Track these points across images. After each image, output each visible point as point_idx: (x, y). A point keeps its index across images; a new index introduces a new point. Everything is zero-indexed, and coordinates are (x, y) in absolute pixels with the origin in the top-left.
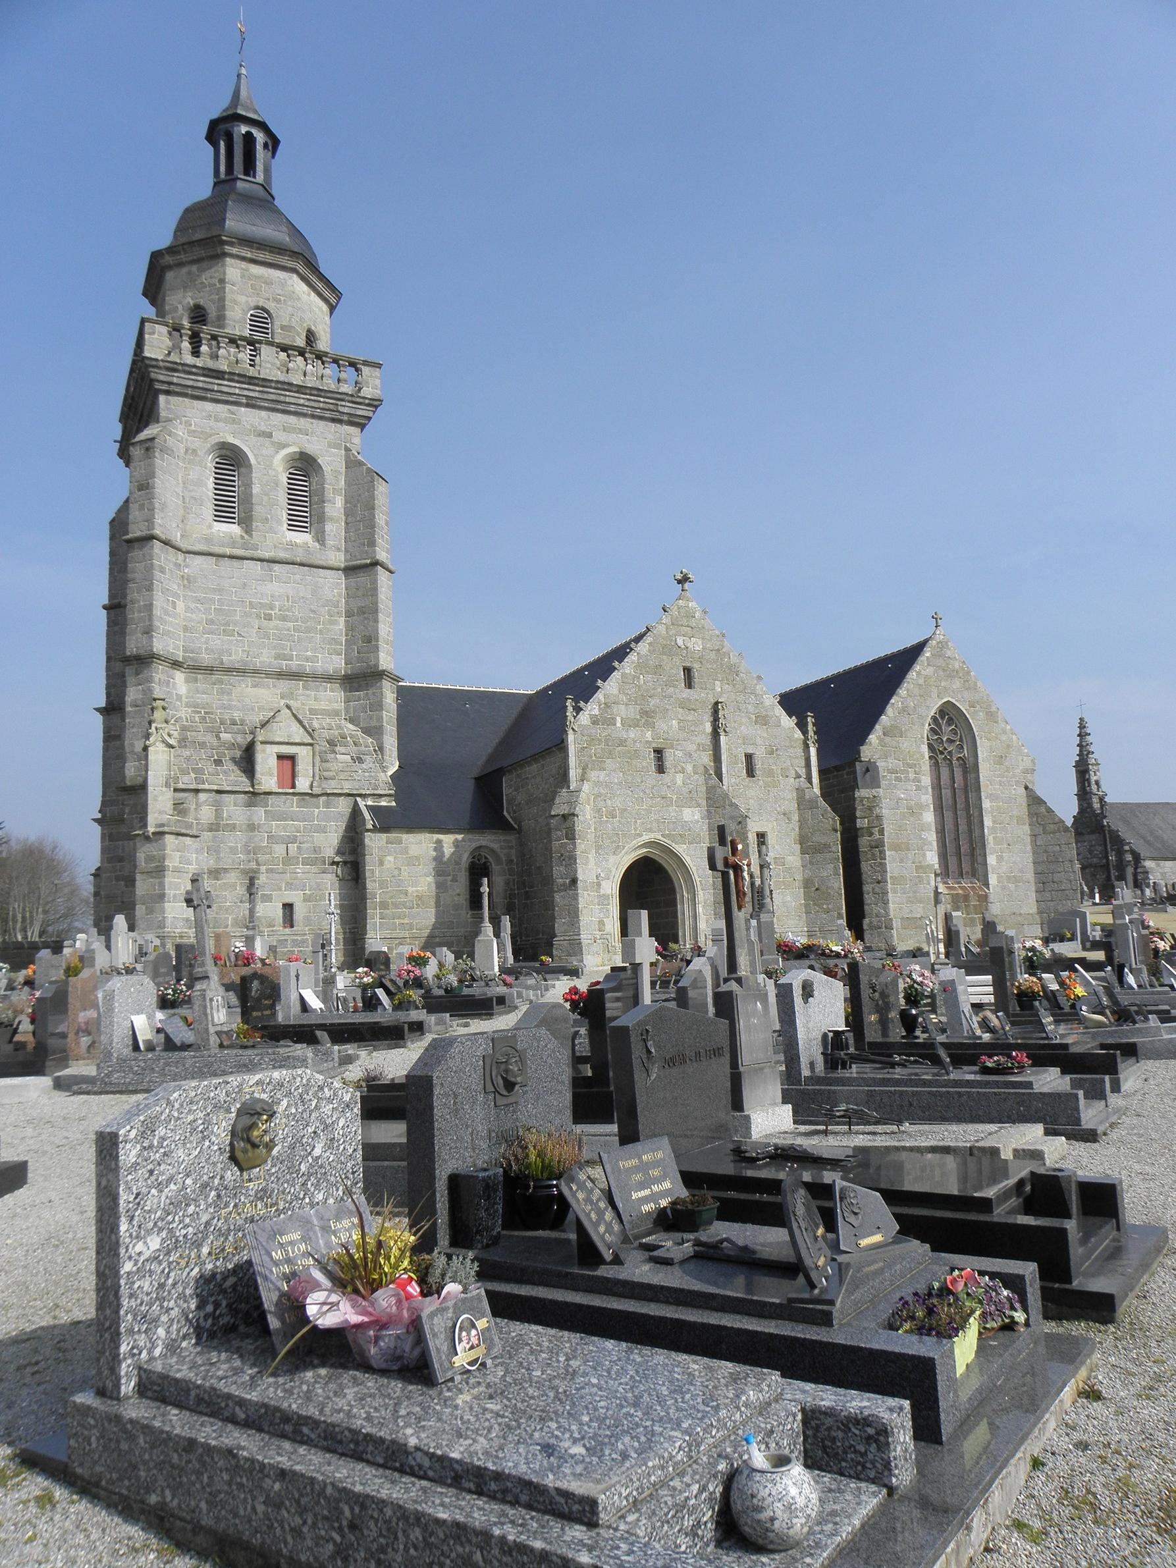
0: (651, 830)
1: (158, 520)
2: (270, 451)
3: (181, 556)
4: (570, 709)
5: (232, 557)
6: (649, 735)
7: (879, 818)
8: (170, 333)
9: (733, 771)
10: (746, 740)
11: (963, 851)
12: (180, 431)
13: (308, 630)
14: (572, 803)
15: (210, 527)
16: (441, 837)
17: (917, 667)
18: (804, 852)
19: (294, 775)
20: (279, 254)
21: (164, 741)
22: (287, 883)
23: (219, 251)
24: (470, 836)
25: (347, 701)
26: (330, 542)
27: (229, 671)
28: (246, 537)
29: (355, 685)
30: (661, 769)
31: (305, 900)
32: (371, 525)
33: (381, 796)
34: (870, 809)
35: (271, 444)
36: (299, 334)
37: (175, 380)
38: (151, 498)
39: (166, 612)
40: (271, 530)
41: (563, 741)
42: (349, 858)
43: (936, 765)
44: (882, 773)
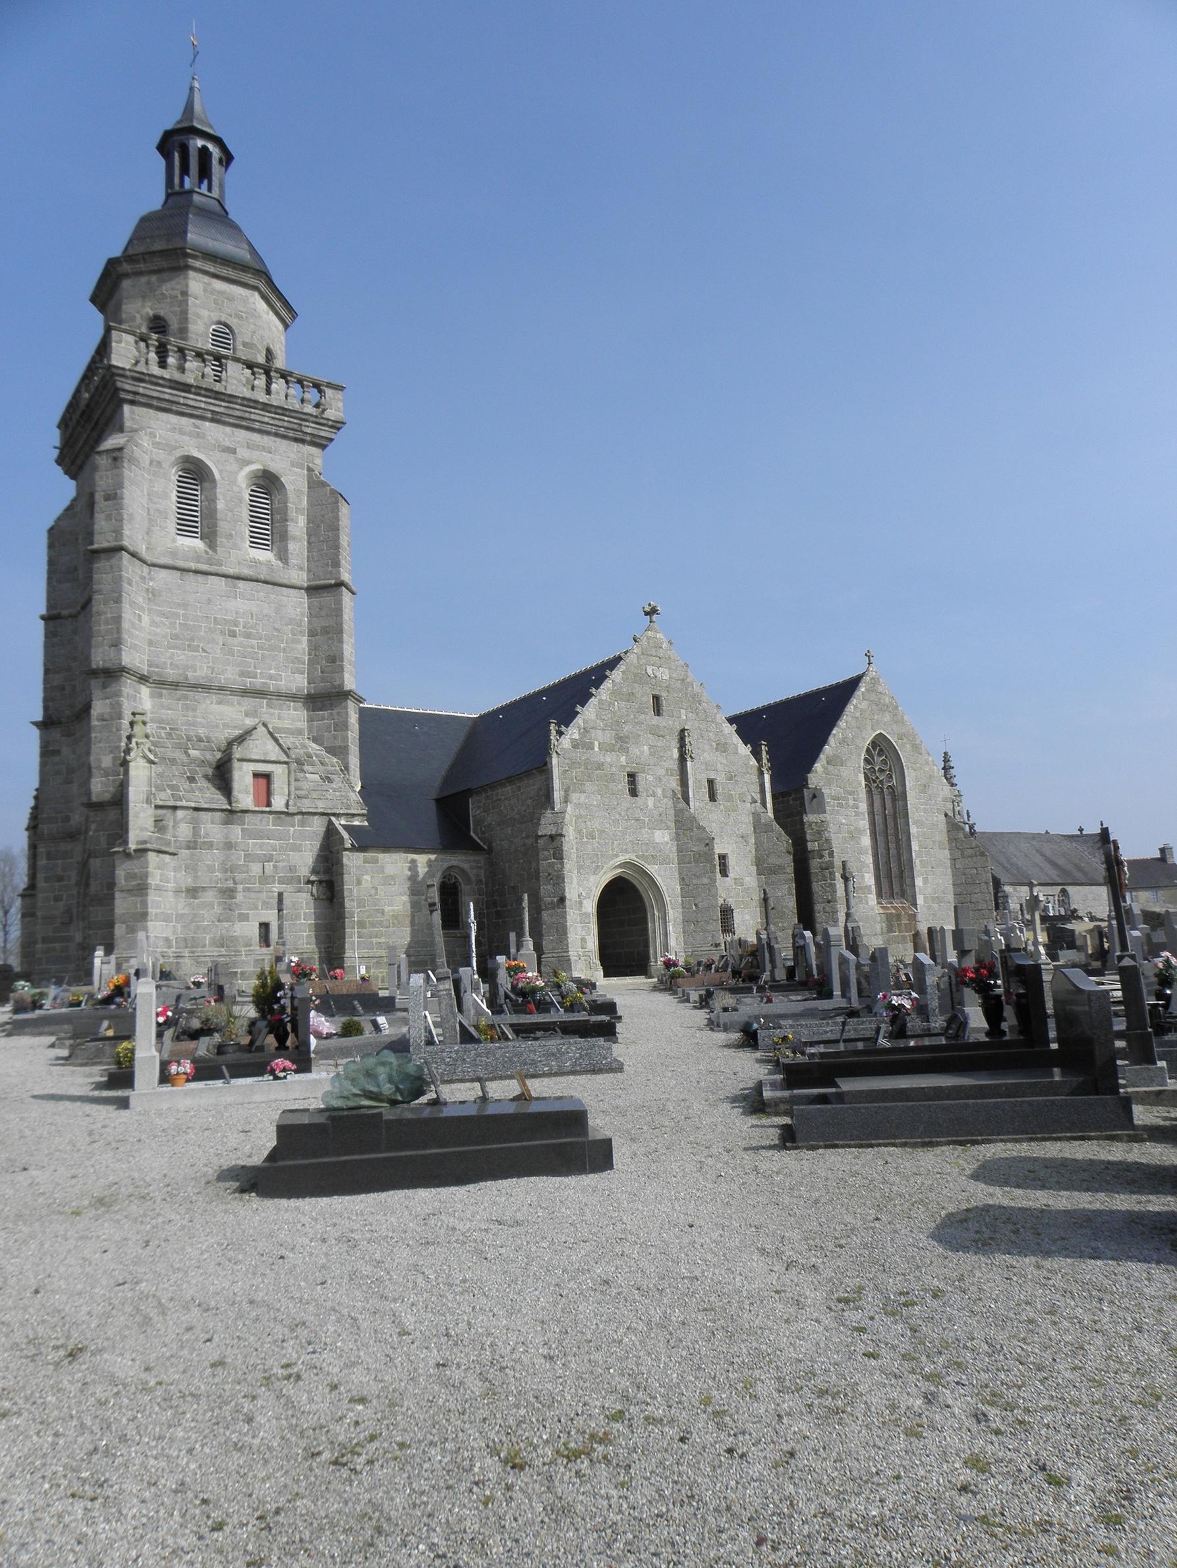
0: (626, 851)
1: (126, 532)
2: (234, 467)
3: (146, 569)
4: (554, 732)
5: (196, 572)
7: (828, 841)
8: (136, 342)
9: (699, 795)
10: (708, 766)
11: (895, 877)
12: (145, 442)
13: (272, 648)
14: (559, 824)
15: (174, 541)
16: (415, 856)
17: (854, 701)
19: (269, 793)
20: (243, 271)
21: (145, 757)
22: (264, 903)
23: (182, 263)
24: (443, 856)
25: (310, 720)
26: (293, 561)
27: (195, 687)
29: (319, 704)
30: (634, 792)
33: (353, 815)
34: (819, 832)
37: (141, 390)
38: (119, 508)
39: (133, 625)
40: (236, 546)
41: (546, 764)
43: (870, 792)
44: (828, 800)
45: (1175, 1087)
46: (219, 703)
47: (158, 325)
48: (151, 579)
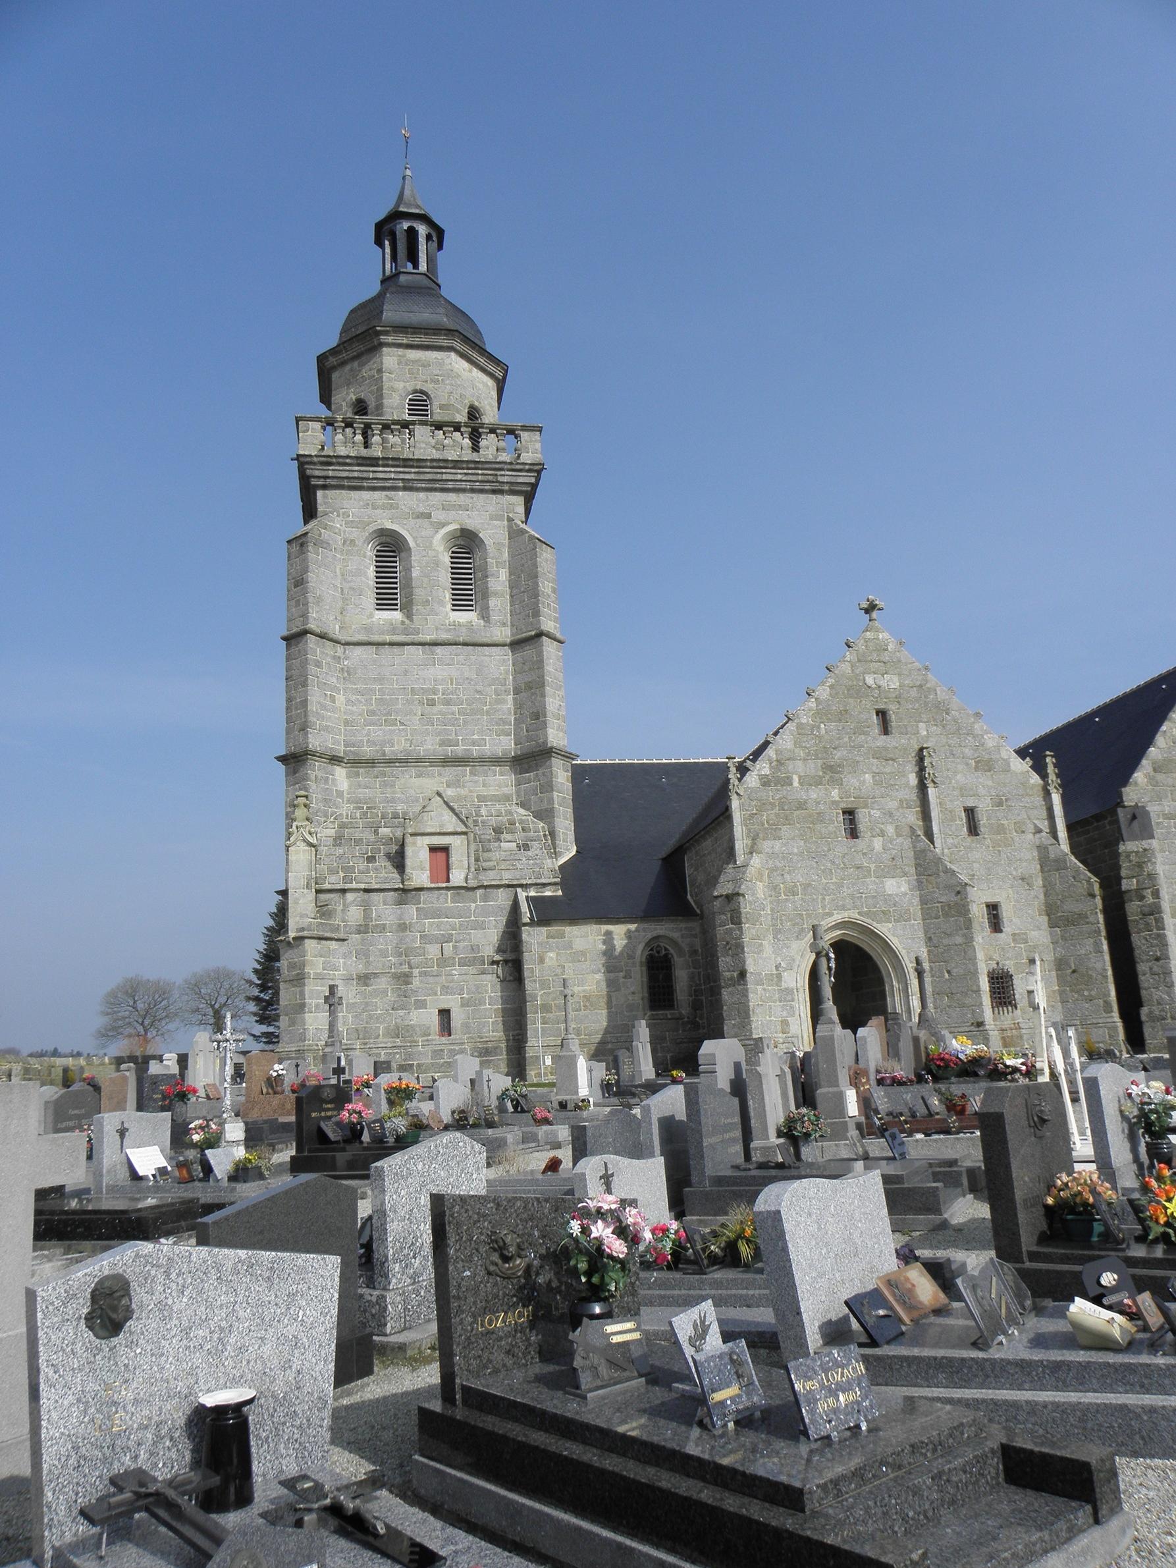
0: (843, 908)
1: (313, 614)
2: (430, 531)
5: (392, 644)
6: (835, 794)
10: (963, 791)
13: (474, 712)
15: (371, 616)
18: (1052, 925)
20: (434, 334)
21: (305, 840)
24: (646, 925)
25: (518, 784)
26: (495, 617)
27: (391, 762)
28: (407, 622)
29: (526, 766)
30: (853, 833)
31: (463, 1005)
32: (535, 594)
33: (544, 885)
34: (1140, 865)
35: (428, 526)
36: (458, 411)
37: (331, 474)
38: (305, 592)
39: (324, 707)
40: (432, 612)
42: (509, 956)
44: (1154, 819)
45: (1174, 1404)
46: (418, 776)
47: (361, 407)
48: (346, 658)
